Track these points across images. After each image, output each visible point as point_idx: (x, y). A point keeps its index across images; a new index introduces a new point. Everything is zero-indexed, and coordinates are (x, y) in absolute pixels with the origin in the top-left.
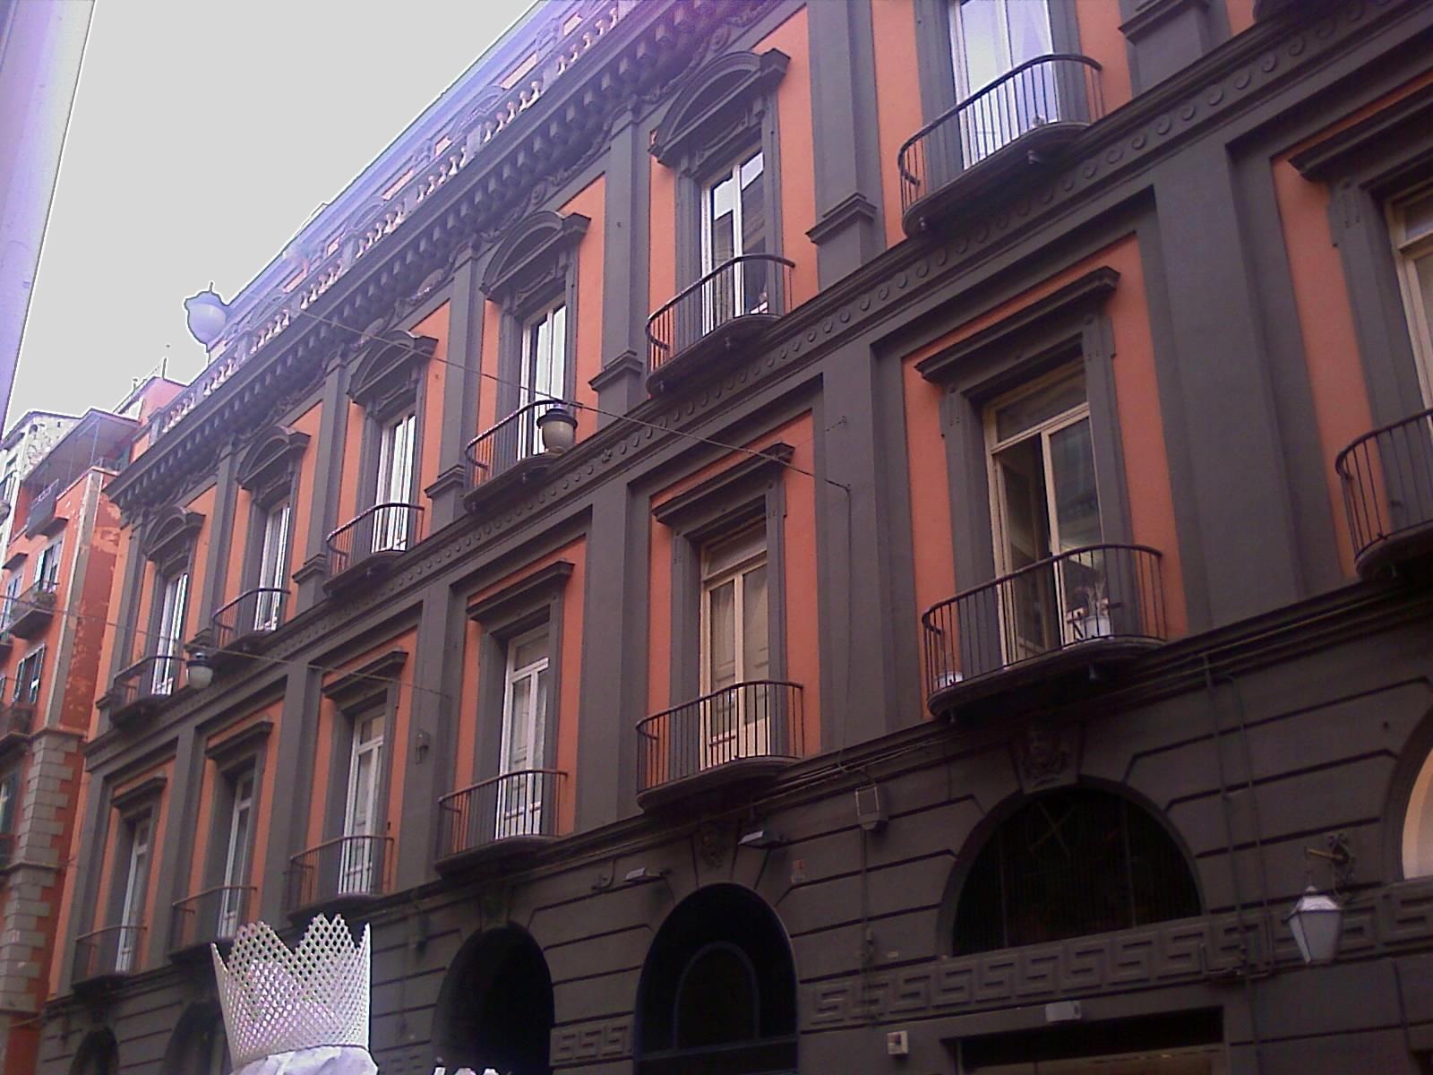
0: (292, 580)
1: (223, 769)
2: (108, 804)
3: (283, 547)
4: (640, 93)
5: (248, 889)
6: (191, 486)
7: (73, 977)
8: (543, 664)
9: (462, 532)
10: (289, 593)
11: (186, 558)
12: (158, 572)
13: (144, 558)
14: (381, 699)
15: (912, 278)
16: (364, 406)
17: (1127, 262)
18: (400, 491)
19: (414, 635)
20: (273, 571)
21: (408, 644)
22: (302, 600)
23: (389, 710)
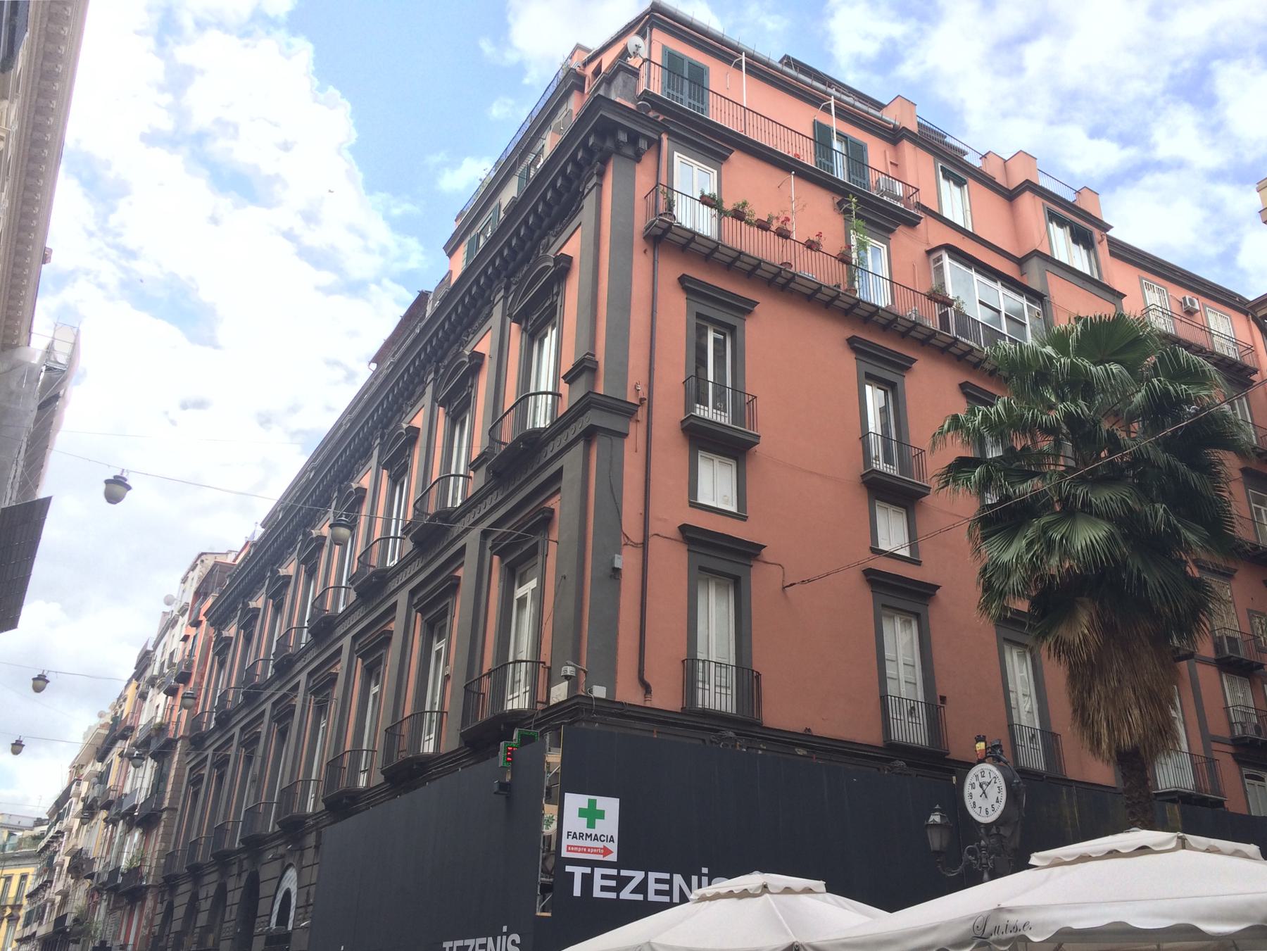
0: (562, 381)
1: (507, 561)
2: (488, 552)
3: (473, 438)
4: (508, 277)
5: (441, 712)
6: (552, 239)
7: (464, 721)
8: (533, 584)
9: (490, 492)
10: (560, 395)
11: (469, 395)
12: (447, 414)
13: (508, 319)
14: (533, 552)
15: (277, 684)
16: (520, 323)
17: (554, 503)
18: (546, 383)
19: (558, 497)
20: (460, 464)
21: (554, 503)
22: (479, 480)
23: (540, 559)
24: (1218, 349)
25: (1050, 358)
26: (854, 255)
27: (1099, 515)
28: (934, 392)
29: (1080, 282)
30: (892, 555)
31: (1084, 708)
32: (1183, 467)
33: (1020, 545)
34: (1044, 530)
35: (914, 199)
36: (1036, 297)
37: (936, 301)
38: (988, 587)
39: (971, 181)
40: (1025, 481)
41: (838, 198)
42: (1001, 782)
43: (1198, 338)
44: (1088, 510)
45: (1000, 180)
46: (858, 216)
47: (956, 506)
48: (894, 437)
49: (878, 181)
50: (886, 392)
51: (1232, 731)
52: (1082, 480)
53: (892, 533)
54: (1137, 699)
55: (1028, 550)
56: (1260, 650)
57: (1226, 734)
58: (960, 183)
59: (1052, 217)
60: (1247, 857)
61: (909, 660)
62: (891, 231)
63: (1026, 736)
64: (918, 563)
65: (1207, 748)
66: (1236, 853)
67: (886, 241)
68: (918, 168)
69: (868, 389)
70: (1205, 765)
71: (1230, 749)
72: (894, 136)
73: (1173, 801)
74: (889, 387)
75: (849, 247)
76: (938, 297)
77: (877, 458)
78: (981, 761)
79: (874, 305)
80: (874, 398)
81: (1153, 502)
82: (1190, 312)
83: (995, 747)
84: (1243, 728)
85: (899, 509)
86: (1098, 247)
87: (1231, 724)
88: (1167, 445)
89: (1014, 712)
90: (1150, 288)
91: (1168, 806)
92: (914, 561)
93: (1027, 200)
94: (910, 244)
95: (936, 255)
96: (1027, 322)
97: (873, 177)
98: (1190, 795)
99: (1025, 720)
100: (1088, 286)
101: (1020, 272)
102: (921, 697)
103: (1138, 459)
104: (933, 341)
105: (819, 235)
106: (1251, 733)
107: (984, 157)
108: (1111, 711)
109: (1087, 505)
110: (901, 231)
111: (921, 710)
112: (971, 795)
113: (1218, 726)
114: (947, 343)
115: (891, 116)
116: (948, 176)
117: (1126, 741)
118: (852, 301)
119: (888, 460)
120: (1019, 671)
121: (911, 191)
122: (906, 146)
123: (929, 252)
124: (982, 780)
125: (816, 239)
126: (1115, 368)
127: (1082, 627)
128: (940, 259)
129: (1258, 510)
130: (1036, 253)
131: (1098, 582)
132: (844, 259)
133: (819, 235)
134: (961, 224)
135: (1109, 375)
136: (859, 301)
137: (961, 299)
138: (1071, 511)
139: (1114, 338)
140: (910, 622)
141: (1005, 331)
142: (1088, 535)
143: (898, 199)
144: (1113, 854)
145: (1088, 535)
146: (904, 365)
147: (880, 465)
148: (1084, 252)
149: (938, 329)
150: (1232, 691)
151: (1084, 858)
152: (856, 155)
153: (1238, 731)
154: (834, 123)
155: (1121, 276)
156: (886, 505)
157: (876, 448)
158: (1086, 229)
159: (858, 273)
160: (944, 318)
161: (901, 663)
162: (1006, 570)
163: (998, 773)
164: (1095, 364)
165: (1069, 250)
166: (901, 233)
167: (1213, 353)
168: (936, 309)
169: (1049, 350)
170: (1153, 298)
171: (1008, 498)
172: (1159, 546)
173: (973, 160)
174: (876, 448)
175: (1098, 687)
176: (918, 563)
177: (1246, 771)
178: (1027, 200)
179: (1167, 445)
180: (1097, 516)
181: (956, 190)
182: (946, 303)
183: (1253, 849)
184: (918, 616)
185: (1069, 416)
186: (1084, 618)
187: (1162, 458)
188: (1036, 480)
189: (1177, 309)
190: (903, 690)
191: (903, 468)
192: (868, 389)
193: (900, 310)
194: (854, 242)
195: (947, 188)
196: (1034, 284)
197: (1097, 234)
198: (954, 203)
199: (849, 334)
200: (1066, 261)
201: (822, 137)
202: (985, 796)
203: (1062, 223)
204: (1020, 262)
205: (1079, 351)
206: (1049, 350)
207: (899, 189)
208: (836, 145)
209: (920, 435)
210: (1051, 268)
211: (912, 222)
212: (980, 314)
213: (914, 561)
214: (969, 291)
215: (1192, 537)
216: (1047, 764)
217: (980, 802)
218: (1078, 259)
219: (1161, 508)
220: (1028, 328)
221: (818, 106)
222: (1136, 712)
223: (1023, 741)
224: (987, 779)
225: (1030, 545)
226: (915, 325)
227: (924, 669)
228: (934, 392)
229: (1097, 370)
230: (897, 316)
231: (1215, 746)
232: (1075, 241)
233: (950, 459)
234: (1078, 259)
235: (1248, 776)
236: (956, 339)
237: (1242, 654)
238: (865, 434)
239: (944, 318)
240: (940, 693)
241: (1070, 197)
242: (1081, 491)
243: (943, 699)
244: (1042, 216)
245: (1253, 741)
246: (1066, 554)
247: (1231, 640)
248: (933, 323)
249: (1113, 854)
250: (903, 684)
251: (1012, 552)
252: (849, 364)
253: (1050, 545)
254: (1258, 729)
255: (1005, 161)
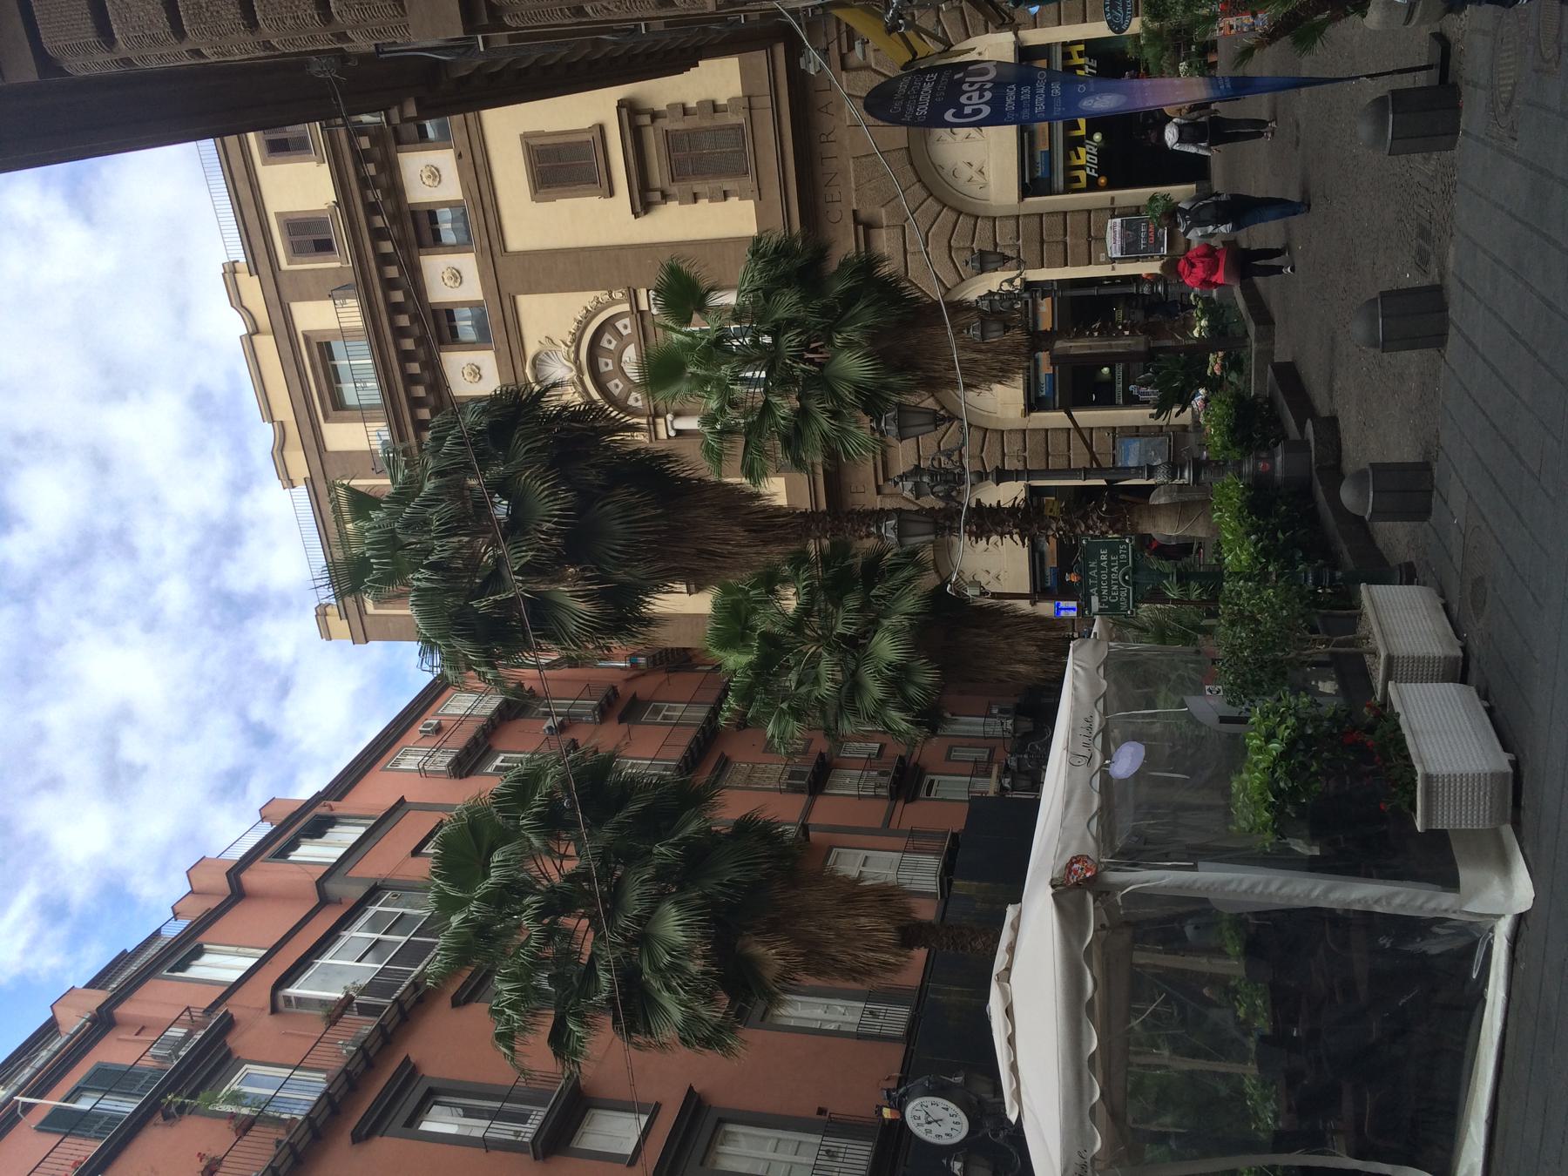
24: (488, 712)
25: (465, 921)
26: (245, 1111)
27: (653, 910)
28: (456, 1042)
29: (371, 841)
30: (645, 1133)
31: (852, 970)
32: (620, 816)
33: (666, 998)
34: (657, 970)
35: (197, 1014)
36: (374, 893)
37: (340, 1016)
38: (707, 1043)
39: (200, 939)
40: (597, 977)
41: (159, 1118)
42: (928, 1100)
43: (470, 730)
44: (645, 918)
45: (213, 903)
46: (193, 1096)
47: (603, 1049)
48: (498, 1105)
49: (154, 1056)
50: (436, 1103)
51: (883, 797)
52: (611, 915)
53: (616, 1132)
54: (849, 916)
55: (675, 992)
56: (805, 752)
57: (883, 805)
58: (199, 952)
59: (283, 854)
60: (1019, 917)
61: (771, 1144)
62: (229, 1054)
63: (869, 1020)
64: (658, 1106)
65: (898, 833)
66: (1015, 928)
67: (240, 1063)
68: (160, 1002)
69: (427, 1126)
70: (915, 841)
71: (900, 804)
72: (103, 1023)
73: (950, 883)
74: (431, 1097)
75: (233, 1116)
76: (335, 1012)
77: (517, 1133)
78: (903, 1116)
79: (320, 1099)
80: (441, 1122)
81: (650, 852)
82: (438, 729)
83: (889, 1096)
84: (881, 786)
85: (588, 1116)
86: (336, 812)
87: (876, 796)
88: (596, 822)
89: (845, 1028)
90: (398, 762)
91: (954, 891)
92: (654, 1111)
93: (250, 879)
94: (255, 1028)
95: (281, 1003)
96: (401, 910)
97: (148, 1062)
98: (945, 865)
99: (853, 1018)
100: (377, 834)
101: (337, 903)
102: (816, 1139)
103: (604, 857)
104: (389, 1030)
105: (201, 1156)
106: (886, 780)
107: (176, 916)
108: (858, 944)
109: (639, 920)
110: (235, 1041)
111: (832, 1142)
112: (939, 1136)
113: (874, 813)
114: (396, 1012)
115: (73, 1022)
116: (183, 965)
117: (889, 936)
118: (305, 1126)
119: (522, 1118)
120: (803, 1010)
121: (186, 1017)
122: (126, 1010)
123: (274, 1010)
124: (923, 1120)
125: (205, 1162)
126: (497, 857)
127: (769, 955)
128: (288, 999)
129: (665, 717)
130: (320, 884)
131: (724, 927)
132: (244, 1127)
133: (201, 1156)
134: (253, 961)
135: (504, 864)
136: (307, 1116)
137: (348, 984)
138: (643, 938)
139: (464, 848)
140: (726, 1133)
141: (404, 939)
142: (672, 926)
143: (189, 1036)
144: (1011, 1041)
145: (672, 926)
146: (409, 1073)
147: (528, 1130)
148: (337, 829)
149: (377, 1020)
150: (844, 787)
151: (1014, 1068)
152: (109, 1080)
153: (884, 792)
154: (50, 1102)
155: (375, 794)
156: (579, 1133)
157: (504, 1131)
158: (313, 820)
159: (270, 1111)
160: (365, 1010)
161: (771, 1155)
162: (692, 1020)
163: (917, 1101)
164: (487, 876)
165: (328, 844)
166: (237, 1042)
167: (490, 718)
168: (351, 1017)
169: (455, 920)
170: (410, 762)
171: (611, 1000)
172: (699, 857)
173: (174, 930)
174: (504, 1131)
175: (832, 951)
176: (658, 1106)
177: (923, 794)
178: (250, 879)
179: (596, 822)
180: (653, 913)
181: (206, 959)
182: (346, 1003)
183: (1011, 911)
184: (721, 1121)
185: (537, 918)
186: (759, 950)
187: (606, 833)
188: (598, 966)
189: (433, 741)
190: (804, 1160)
191: (537, 1099)
192: (427, 1126)
193: (337, 1064)
194: (229, 1108)
195: (197, 971)
196: (358, 892)
197: (321, 810)
198: (222, 965)
199: (345, 1139)
200: (342, 851)
201: (65, 1123)
202: (937, 1120)
203: (294, 845)
204: (324, 901)
205: (465, 884)
206: (455, 920)
207: (178, 1032)
208: (84, 1104)
209: (496, 1069)
210: (344, 869)
211: (228, 1024)
212: (371, 966)
213: (654, 1111)
214: (341, 971)
215: (692, 828)
216: (902, 1003)
217: (942, 1130)
218: (344, 836)
219: (658, 849)
220: (407, 911)
221: (18, 1119)
222: (863, 920)
223: (875, 1027)
224: (922, 1115)
225: (669, 988)
226: (362, 1048)
227: (784, 1128)
228: (456, 1042)
229: (495, 875)
230: (344, 1070)
231: (894, 825)
232: (320, 834)
233: (549, 1051)
234: (344, 836)
235: (928, 794)
236: (397, 1000)
237: (808, 769)
238: (485, 1144)
239: (365, 1010)
240: (813, 1114)
241: (266, 828)
242: (622, 922)
243: (821, 1111)
244: (278, 866)
245: (894, 780)
246: (688, 953)
247: (792, 776)
248: (367, 1026)
249: (1011, 1041)
250: (797, 1159)
251: (673, 1009)
252: (385, 1147)
253: (675, 968)
254: (882, 774)
255: (192, 892)
